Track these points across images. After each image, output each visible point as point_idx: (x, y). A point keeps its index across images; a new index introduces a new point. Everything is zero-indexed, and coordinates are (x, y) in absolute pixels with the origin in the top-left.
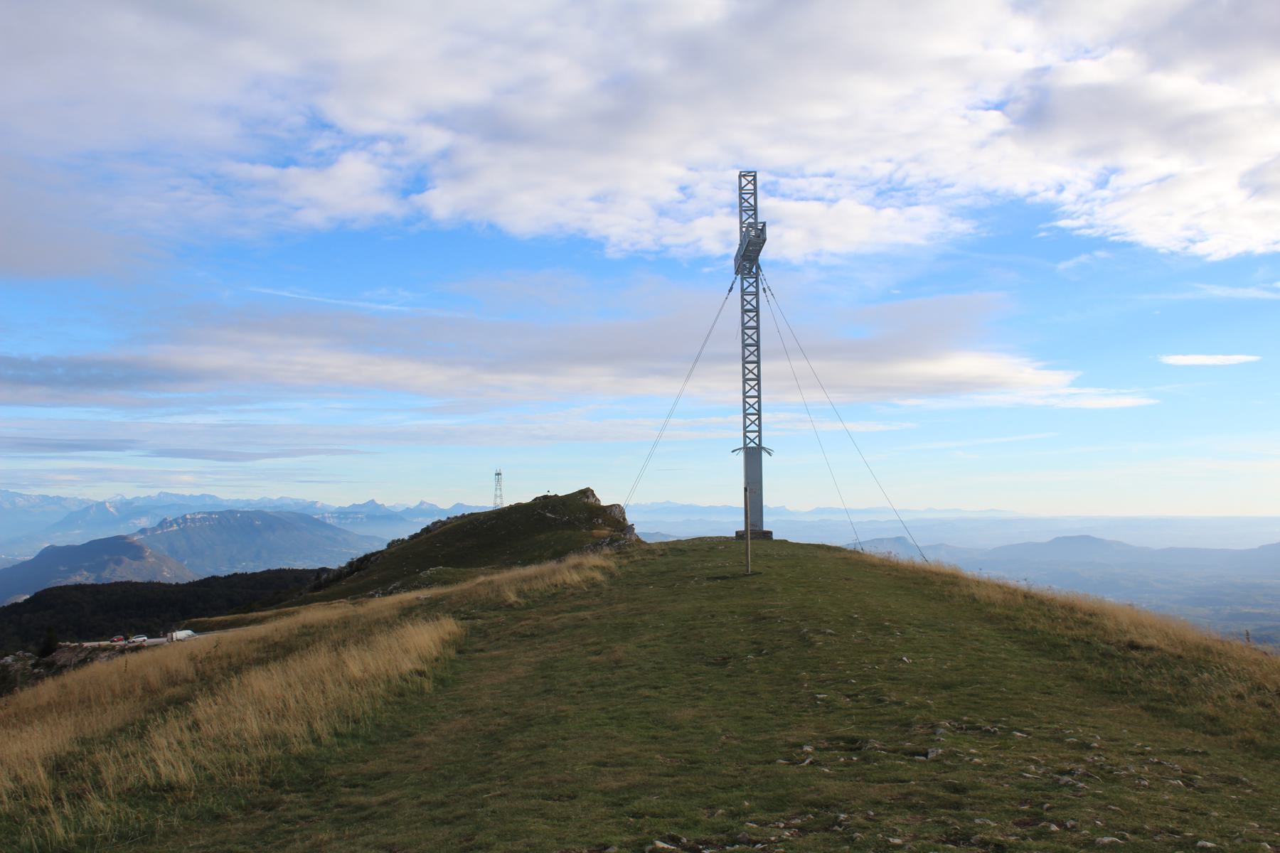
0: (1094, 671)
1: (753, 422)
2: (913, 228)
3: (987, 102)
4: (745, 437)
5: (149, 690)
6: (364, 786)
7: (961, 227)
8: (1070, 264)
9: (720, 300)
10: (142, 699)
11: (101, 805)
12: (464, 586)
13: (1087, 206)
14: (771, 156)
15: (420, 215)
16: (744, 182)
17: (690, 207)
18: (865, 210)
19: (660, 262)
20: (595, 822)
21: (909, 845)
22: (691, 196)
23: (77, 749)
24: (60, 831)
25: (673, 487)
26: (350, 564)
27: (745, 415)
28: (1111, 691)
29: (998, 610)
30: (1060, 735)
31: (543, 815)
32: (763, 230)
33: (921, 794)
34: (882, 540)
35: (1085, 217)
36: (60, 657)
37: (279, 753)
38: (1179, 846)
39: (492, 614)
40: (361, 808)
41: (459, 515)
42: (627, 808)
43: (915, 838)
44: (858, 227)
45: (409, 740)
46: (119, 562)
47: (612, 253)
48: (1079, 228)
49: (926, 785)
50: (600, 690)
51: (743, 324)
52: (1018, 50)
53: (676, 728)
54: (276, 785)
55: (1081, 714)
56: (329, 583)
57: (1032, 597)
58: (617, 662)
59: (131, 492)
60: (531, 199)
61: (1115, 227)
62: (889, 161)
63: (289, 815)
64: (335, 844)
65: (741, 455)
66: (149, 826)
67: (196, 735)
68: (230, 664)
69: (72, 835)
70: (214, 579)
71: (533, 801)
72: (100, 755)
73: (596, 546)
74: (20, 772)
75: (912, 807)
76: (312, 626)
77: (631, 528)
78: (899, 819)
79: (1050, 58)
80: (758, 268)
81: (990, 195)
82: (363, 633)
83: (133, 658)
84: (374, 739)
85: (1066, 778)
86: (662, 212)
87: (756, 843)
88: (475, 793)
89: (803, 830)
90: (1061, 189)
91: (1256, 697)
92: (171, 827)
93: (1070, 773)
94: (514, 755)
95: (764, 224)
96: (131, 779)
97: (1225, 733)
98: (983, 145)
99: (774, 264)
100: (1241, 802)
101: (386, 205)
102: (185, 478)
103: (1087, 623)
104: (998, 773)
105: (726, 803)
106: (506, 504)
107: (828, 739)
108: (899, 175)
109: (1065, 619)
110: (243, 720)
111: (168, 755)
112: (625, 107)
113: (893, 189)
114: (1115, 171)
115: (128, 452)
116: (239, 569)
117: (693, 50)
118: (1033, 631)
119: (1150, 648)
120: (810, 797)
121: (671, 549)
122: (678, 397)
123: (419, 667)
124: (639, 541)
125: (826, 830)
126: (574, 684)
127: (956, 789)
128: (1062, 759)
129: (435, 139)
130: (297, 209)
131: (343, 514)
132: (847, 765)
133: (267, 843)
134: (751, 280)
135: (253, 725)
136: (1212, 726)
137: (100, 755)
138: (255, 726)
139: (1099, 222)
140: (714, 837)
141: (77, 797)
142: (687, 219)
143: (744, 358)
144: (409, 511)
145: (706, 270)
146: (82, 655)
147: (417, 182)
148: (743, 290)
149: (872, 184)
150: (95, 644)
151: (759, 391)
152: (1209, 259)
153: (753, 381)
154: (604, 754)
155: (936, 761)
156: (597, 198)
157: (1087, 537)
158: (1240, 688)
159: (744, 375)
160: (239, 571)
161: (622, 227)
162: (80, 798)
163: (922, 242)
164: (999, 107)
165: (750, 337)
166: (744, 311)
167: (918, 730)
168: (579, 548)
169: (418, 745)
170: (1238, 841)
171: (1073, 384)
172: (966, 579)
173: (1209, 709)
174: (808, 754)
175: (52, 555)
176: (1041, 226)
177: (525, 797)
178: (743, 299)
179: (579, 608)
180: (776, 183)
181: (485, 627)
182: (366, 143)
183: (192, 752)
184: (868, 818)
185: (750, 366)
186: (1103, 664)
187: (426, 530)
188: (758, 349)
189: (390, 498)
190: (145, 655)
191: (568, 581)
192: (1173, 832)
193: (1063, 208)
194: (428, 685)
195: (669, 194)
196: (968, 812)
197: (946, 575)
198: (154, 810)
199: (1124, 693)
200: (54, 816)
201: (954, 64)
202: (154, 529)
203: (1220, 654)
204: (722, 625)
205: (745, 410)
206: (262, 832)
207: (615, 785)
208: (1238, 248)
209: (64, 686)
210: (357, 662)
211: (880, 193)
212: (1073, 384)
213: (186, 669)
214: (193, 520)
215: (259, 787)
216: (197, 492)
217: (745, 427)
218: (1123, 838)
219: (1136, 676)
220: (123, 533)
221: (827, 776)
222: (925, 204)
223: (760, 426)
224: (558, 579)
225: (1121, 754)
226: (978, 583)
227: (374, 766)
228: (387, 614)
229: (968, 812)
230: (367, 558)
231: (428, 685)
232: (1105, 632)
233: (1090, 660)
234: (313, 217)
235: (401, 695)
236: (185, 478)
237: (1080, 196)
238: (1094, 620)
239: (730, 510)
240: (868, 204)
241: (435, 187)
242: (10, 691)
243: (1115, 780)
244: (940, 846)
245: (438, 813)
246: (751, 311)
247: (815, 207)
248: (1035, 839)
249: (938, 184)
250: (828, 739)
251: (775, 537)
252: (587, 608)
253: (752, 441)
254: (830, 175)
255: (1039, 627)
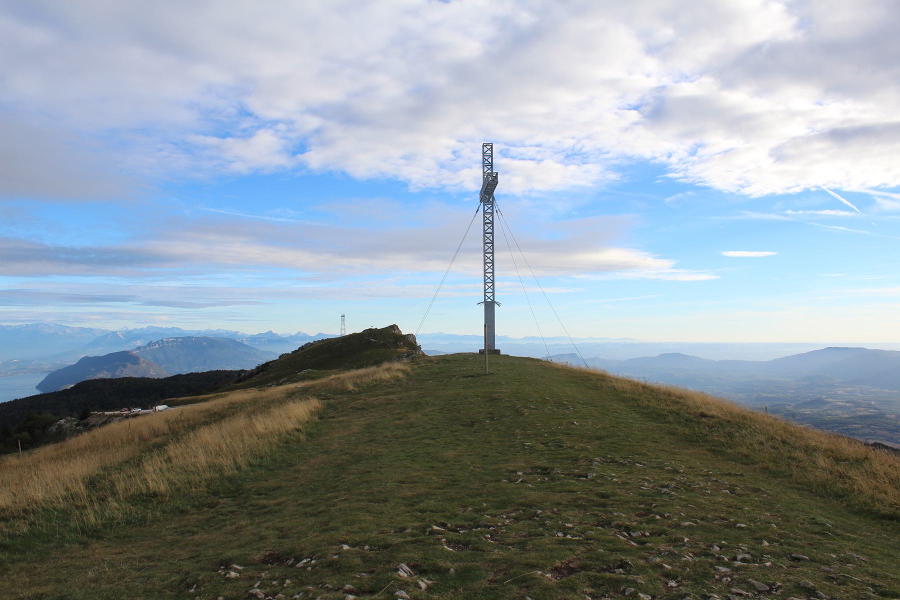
0: (680, 429)
2: (585, 177)
3: (629, 105)
4: (485, 295)
5: (142, 439)
6: (266, 494)
7: (613, 176)
9: (471, 215)
10: (139, 445)
11: (116, 505)
12: (324, 380)
13: (684, 166)
14: (503, 134)
15: (302, 166)
16: (486, 149)
17: (459, 162)
18: (559, 166)
19: (441, 194)
20: (398, 515)
21: (577, 527)
22: (459, 157)
23: (102, 473)
24: (93, 520)
25: (444, 325)
26: (258, 368)
27: (485, 283)
28: (691, 441)
30: (661, 465)
31: (368, 511)
32: (496, 177)
33: (583, 499)
36: (92, 420)
37: (217, 475)
38: (727, 526)
39: (339, 396)
40: (264, 507)
42: (416, 507)
43: (580, 523)
44: (555, 176)
45: (292, 468)
46: (125, 366)
47: (412, 189)
49: (587, 494)
50: (401, 440)
51: (484, 231)
52: (648, 76)
53: (445, 462)
54: (216, 493)
55: (673, 453)
56: (245, 378)
58: (411, 424)
59: (131, 326)
61: (700, 178)
62: (573, 138)
63: (223, 511)
64: (249, 527)
66: (143, 517)
67: (170, 465)
68: (189, 425)
69: (99, 521)
70: (180, 376)
71: (363, 503)
72: (115, 476)
73: (399, 358)
74: (69, 486)
75: (578, 506)
78: (571, 513)
79: (666, 81)
80: (493, 199)
81: (629, 158)
82: (265, 407)
83: (133, 421)
84: (271, 468)
85: (665, 490)
86: (442, 166)
87: (489, 527)
88: (329, 499)
89: (517, 519)
90: (670, 156)
91: (770, 443)
92: (156, 517)
93: (667, 486)
94: (352, 477)
96: (133, 490)
97: (753, 464)
98: (626, 130)
99: (506, 196)
100: (761, 502)
101: (283, 161)
102: (163, 318)
103: (678, 403)
104: (627, 487)
105: (472, 504)
106: (347, 334)
107: (531, 468)
108: (578, 146)
109: (665, 400)
110: (196, 457)
111: (154, 476)
112: (423, 105)
113: (575, 154)
114: (700, 146)
115: (131, 303)
116: (194, 370)
117: (463, 73)
118: (648, 407)
119: (713, 417)
120: (521, 501)
121: (442, 360)
122: (447, 272)
124: (424, 355)
125: (530, 519)
126: (386, 437)
127: (603, 496)
128: (663, 479)
129: (312, 122)
131: (253, 339)
132: (542, 482)
133: (211, 526)
135: (202, 459)
136: (746, 460)
137: (115, 476)
138: (203, 460)
140: (466, 523)
141: (103, 500)
142: (456, 170)
143: (485, 251)
145: (466, 199)
146: (104, 419)
147: (301, 147)
148: (484, 211)
149: (564, 151)
150: (112, 413)
151: (493, 269)
152: (752, 197)
153: (489, 263)
154: (404, 476)
155: (592, 480)
156: (405, 158)
158: (762, 438)
160: (194, 371)
161: (418, 174)
162: (103, 500)
163: (590, 185)
164: (636, 108)
166: (485, 224)
167: (582, 463)
168: (390, 359)
169: (297, 471)
170: (759, 524)
171: (674, 267)
172: (610, 377)
173: (744, 450)
174: (520, 476)
175: (87, 362)
177: (358, 501)
178: (484, 217)
179: (390, 393)
180: (507, 150)
181: (335, 404)
183: (168, 475)
184: (553, 512)
185: (488, 255)
186: (686, 426)
187: (301, 348)
189: (281, 330)
190: (140, 420)
192: (723, 519)
194: (302, 437)
195: (446, 155)
196: (610, 509)
197: (599, 375)
198: (146, 507)
199: (697, 441)
200: (89, 509)
201: (612, 83)
202: (145, 347)
203: (751, 420)
204: (471, 403)
206: (208, 521)
207: (409, 494)
208: (768, 191)
209: (94, 437)
210: (261, 424)
212: (674, 267)
213: (165, 428)
214: (167, 342)
215: (206, 495)
216: (170, 326)
218: (696, 522)
219: (704, 432)
220: (127, 349)
221: (531, 489)
223: (493, 289)
224: (377, 376)
225: (696, 476)
226: (617, 380)
227: (272, 483)
228: (279, 396)
229: (610, 509)
230: (267, 364)
231: (302, 437)
232: (688, 407)
233: (679, 423)
234: (240, 167)
235: (287, 442)
236: (163, 318)
238: (682, 400)
239: (476, 337)
240: (561, 162)
242: (64, 439)
243: (692, 490)
244: (594, 528)
245: (309, 510)
246: (489, 223)
247: (530, 164)
248: (647, 523)
249: (600, 151)
250: (531, 468)
252: (394, 393)
255: (651, 404)
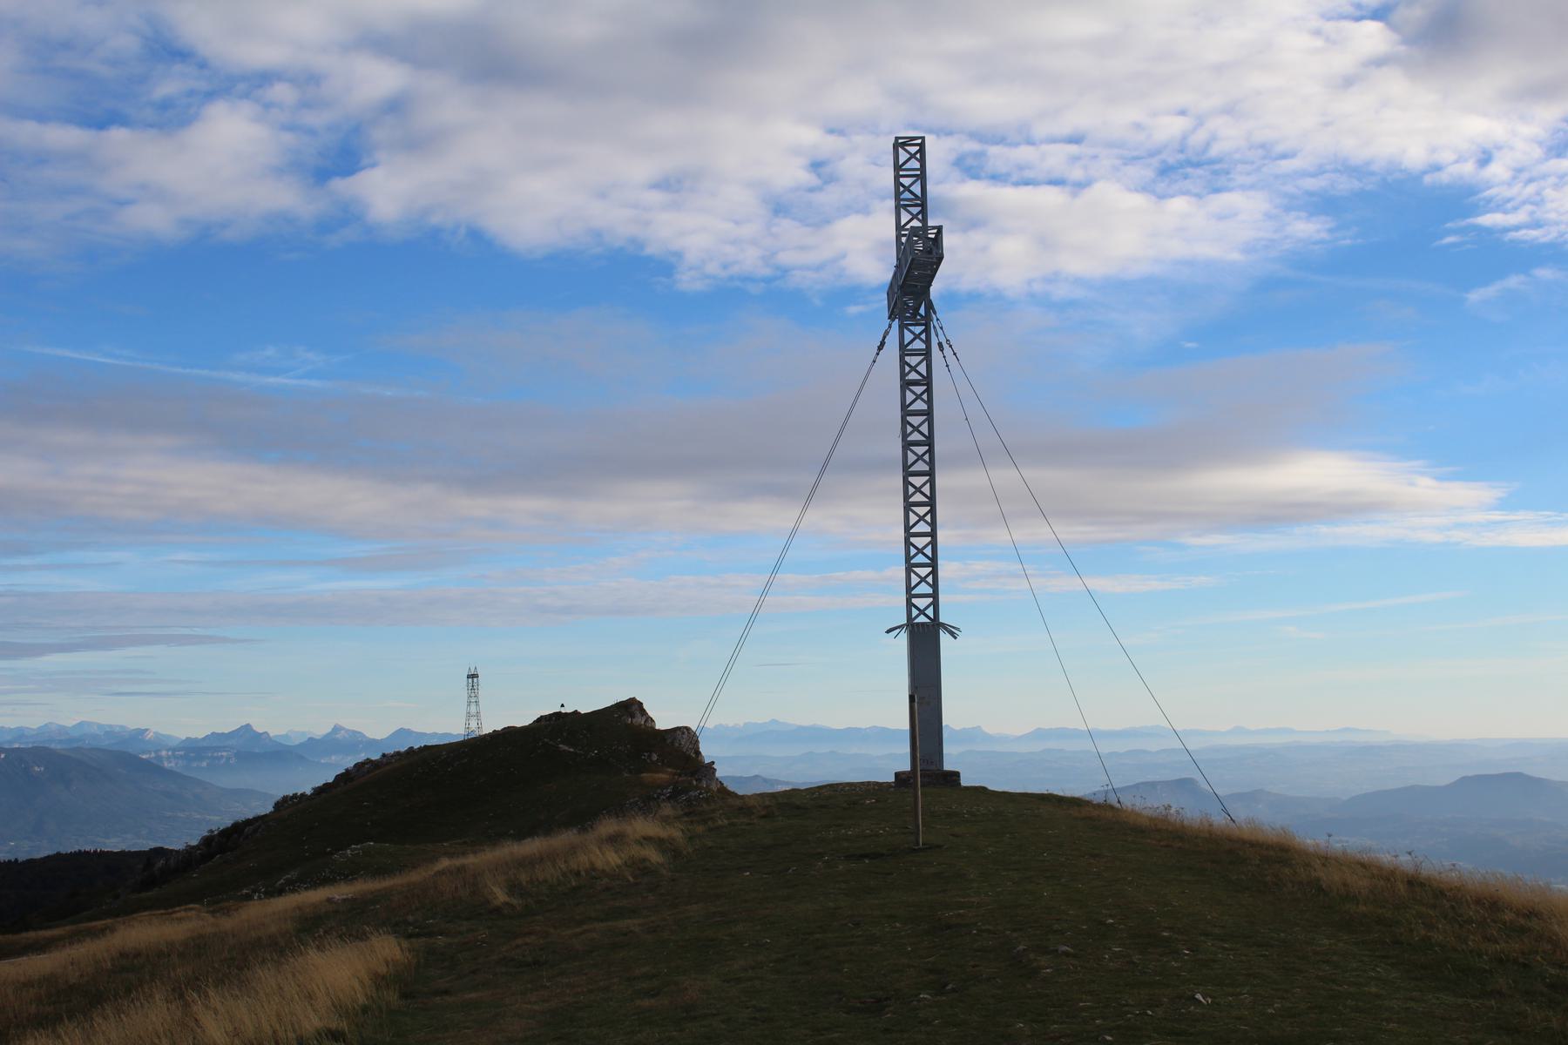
1: (923, 579)
2: (1217, 231)
3: (1358, 6)
4: (910, 605)
7: (1307, 228)
8: (1490, 291)
12: (416, 876)
13: (1531, 189)
15: (348, 214)
17: (829, 198)
18: (1139, 200)
19: (736, 297)
22: (831, 179)
26: (207, 841)
27: (910, 568)
29: (1362, 908)
34: (1153, 784)
35: (1529, 208)
41: (403, 749)
44: (1127, 231)
47: (687, 282)
48: (1517, 228)
57: (1422, 885)
60: (540, 183)
65: (903, 639)
73: (647, 803)
76: (138, 955)
77: (710, 768)
80: (930, 306)
82: (231, 963)
90: (1485, 159)
95: (940, 229)
98: (1348, 82)
99: (952, 298)
108: (1200, 137)
123: (333, 1026)
124: (724, 791)
130: (123, 203)
131: (194, 750)
134: (918, 329)
139: (1553, 216)
142: (820, 221)
143: (906, 467)
144: (312, 744)
145: (853, 310)
147: (343, 156)
148: (903, 347)
149: (1153, 154)
153: (921, 503)
157: (1519, 775)
159: (906, 496)
161: (701, 235)
163: (1235, 256)
165: (916, 429)
166: (906, 384)
168: (618, 808)
176: (1449, 225)
178: (903, 363)
180: (980, 155)
182: (248, 85)
185: (917, 481)
188: (931, 451)
191: (599, 864)
193: (1487, 193)
195: (793, 174)
205: (908, 558)
211: (1165, 171)
212: (1503, 505)
217: (909, 589)
222: (1243, 188)
223: (935, 586)
224: (582, 860)
226: (1326, 860)
228: (273, 929)
230: (238, 829)
234: (151, 219)
237: (1518, 171)
239: (882, 734)
240: (1144, 189)
241: (373, 165)
246: (917, 384)
247: (1050, 197)
249: (1269, 152)
251: (964, 782)
253: (922, 612)
254: (1075, 139)
